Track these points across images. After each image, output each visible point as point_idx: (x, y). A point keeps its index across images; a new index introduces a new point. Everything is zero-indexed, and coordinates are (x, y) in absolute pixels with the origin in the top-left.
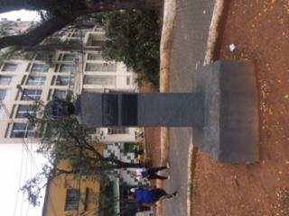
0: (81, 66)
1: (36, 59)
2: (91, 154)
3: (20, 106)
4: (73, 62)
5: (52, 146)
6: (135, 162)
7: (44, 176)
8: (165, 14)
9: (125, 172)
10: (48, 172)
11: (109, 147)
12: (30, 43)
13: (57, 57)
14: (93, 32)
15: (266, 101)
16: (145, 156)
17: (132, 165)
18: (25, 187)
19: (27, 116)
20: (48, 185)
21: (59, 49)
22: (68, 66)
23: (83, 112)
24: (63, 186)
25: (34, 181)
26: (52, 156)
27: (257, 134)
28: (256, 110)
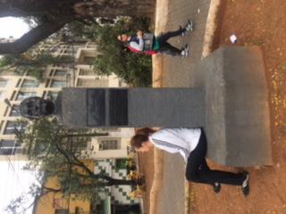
0: (72, 81)
1: (27, 75)
2: (80, 170)
3: (8, 122)
4: (64, 78)
5: (40, 163)
6: (127, 179)
7: (30, 195)
8: (157, 19)
9: (117, 189)
10: (35, 190)
11: (100, 164)
12: (15, 54)
13: (49, 73)
14: (85, 49)
15: (279, 92)
16: (138, 172)
17: (124, 182)
18: (10, 207)
19: (15, 132)
20: (36, 203)
21: (50, 63)
22: (57, 81)
23: (64, 111)
24: (50, 206)
25: (19, 200)
26: (40, 174)
27: (268, 132)
28: (267, 105)
